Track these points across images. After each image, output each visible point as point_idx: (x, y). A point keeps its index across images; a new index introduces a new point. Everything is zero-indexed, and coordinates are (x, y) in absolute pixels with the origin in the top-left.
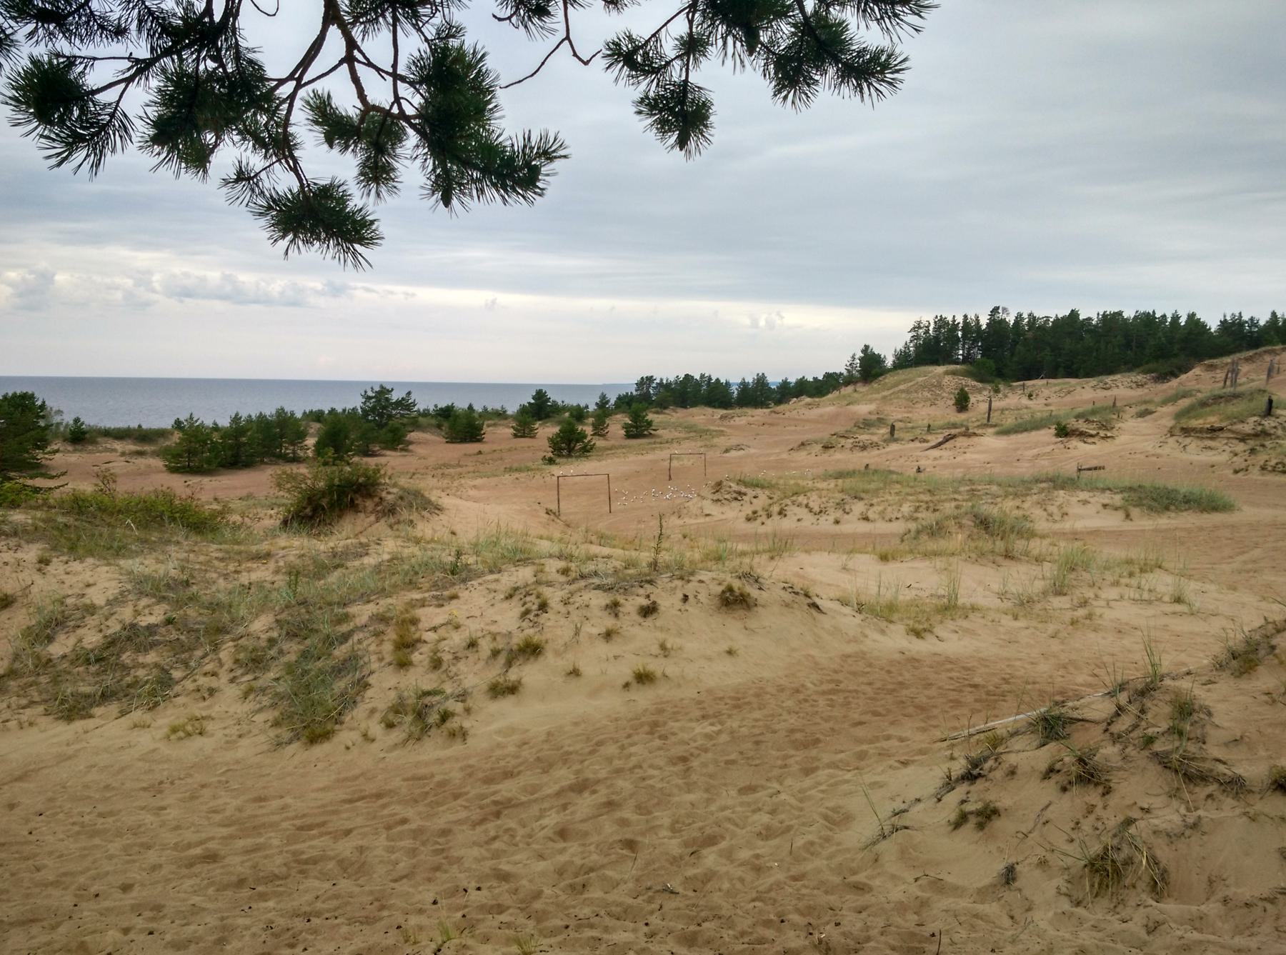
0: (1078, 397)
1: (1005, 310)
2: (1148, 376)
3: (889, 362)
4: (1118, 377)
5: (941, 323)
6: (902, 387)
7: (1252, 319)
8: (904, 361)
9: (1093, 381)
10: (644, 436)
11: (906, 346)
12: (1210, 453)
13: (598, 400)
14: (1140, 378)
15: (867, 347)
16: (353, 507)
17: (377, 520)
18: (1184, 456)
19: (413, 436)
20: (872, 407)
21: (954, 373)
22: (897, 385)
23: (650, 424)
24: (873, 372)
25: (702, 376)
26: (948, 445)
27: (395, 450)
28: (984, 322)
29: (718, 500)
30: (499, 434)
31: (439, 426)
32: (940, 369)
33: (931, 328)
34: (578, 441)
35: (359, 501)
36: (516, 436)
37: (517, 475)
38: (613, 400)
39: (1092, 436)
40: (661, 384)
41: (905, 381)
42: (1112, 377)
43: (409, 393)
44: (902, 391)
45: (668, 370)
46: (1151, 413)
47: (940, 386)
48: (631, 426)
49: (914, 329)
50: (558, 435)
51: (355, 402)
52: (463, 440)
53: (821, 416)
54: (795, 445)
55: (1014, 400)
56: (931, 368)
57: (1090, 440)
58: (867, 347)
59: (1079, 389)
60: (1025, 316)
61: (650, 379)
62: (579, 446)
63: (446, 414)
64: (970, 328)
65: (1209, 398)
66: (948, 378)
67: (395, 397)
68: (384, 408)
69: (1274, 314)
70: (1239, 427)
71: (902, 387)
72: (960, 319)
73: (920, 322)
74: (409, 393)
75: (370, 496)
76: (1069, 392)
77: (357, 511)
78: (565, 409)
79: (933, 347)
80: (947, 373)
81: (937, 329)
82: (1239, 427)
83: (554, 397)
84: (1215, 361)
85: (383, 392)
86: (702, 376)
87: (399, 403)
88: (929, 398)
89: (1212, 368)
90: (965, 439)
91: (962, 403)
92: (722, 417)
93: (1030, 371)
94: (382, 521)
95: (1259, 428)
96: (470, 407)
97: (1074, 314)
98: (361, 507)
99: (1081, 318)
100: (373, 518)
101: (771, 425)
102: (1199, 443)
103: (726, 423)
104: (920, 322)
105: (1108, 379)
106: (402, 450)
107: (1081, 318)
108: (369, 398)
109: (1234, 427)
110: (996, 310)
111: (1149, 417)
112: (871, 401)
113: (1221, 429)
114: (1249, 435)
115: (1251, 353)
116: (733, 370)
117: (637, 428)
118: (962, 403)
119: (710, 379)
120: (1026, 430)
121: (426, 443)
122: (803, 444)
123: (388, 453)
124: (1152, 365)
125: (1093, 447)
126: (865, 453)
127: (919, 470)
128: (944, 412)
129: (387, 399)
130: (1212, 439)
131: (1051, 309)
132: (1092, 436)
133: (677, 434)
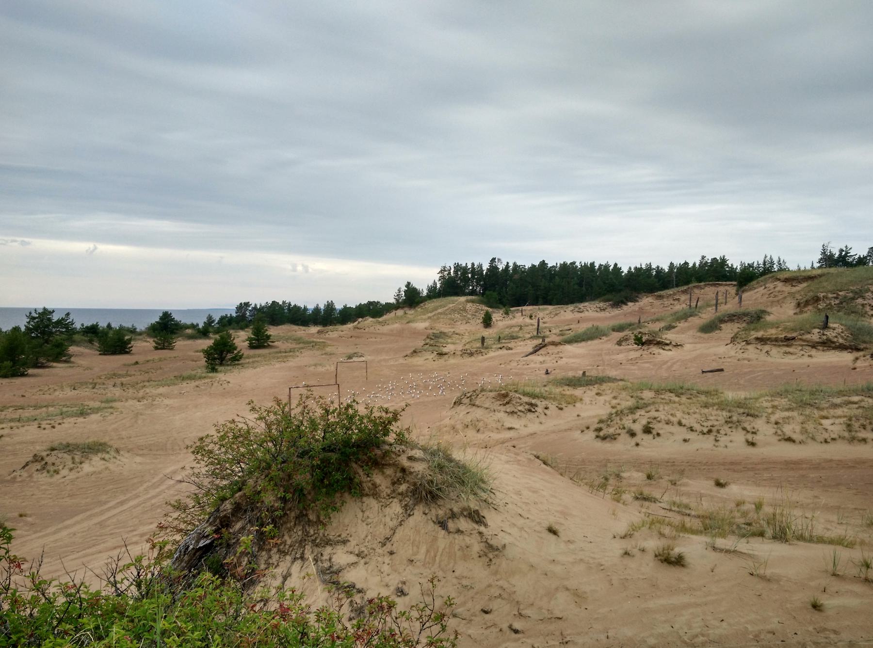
0: (563, 318)
1: (499, 260)
2: (607, 304)
3: (425, 293)
4: (586, 304)
5: (458, 267)
6: (440, 311)
7: (658, 267)
8: (434, 293)
9: (571, 307)
10: (264, 347)
11: (435, 283)
12: (790, 356)
13: (205, 320)
14: (601, 304)
15: (409, 283)
16: (353, 488)
17: (408, 511)
18: (769, 359)
19: (72, 349)
20: (426, 324)
21: (473, 301)
22: (436, 309)
23: (268, 337)
24: (416, 300)
25: (284, 302)
26: (542, 351)
27: (59, 362)
28: (486, 267)
29: (513, 413)
30: (143, 346)
31: (91, 341)
32: (463, 299)
33: (452, 271)
34: (229, 352)
35: (361, 475)
36: (156, 348)
37: (197, 383)
38: (217, 318)
39: (667, 344)
40: (255, 308)
41: (441, 306)
42: (582, 305)
43: (68, 314)
44: (441, 314)
45: (260, 298)
46: (674, 327)
47: (465, 310)
48: (254, 339)
49: (441, 272)
50: (211, 347)
51: (22, 324)
52: (114, 353)
53: (392, 331)
54: (409, 352)
55: (521, 318)
56: (456, 298)
57: (667, 348)
58: (409, 283)
59: (562, 312)
60: (511, 265)
61: (247, 304)
62: (229, 356)
63: (93, 330)
64: (476, 271)
65: (724, 316)
66: (469, 305)
67: (55, 318)
68: (47, 326)
69: (671, 264)
70: (808, 336)
71: (440, 311)
72: (469, 266)
73: (445, 267)
74: (68, 314)
75: (377, 464)
76: (556, 314)
77: (362, 494)
78: (187, 327)
79: (455, 283)
80: (468, 301)
81: (456, 272)
82: (808, 336)
83: (177, 317)
84: (662, 293)
85: (46, 313)
86: (284, 302)
87: (59, 322)
88: (463, 319)
89: (660, 297)
90: (553, 347)
91: (487, 322)
92: (319, 332)
93: (519, 301)
94: (418, 514)
95: (825, 337)
96: (109, 326)
97: (543, 263)
98: (366, 486)
99: (549, 266)
100: (396, 508)
101: (358, 337)
102: (779, 349)
103: (322, 336)
104: (445, 267)
105: (581, 305)
106: (65, 362)
107: (549, 266)
108: (34, 318)
109: (804, 337)
110: (493, 260)
111: (673, 330)
112: (425, 320)
113: (794, 339)
114: (818, 343)
115: (686, 287)
116: (309, 299)
117: (258, 340)
118: (487, 322)
119: (290, 304)
120: (576, 341)
121: (81, 355)
122: (415, 352)
123: (55, 364)
124: (606, 297)
125: (670, 353)
126: (473, 359)
127: (547, 373)
128: (475, 327)
129: (49, 320)
130: (787, 346)
131: (527, 262)
132: (667, 344)
133: (294, 346)
